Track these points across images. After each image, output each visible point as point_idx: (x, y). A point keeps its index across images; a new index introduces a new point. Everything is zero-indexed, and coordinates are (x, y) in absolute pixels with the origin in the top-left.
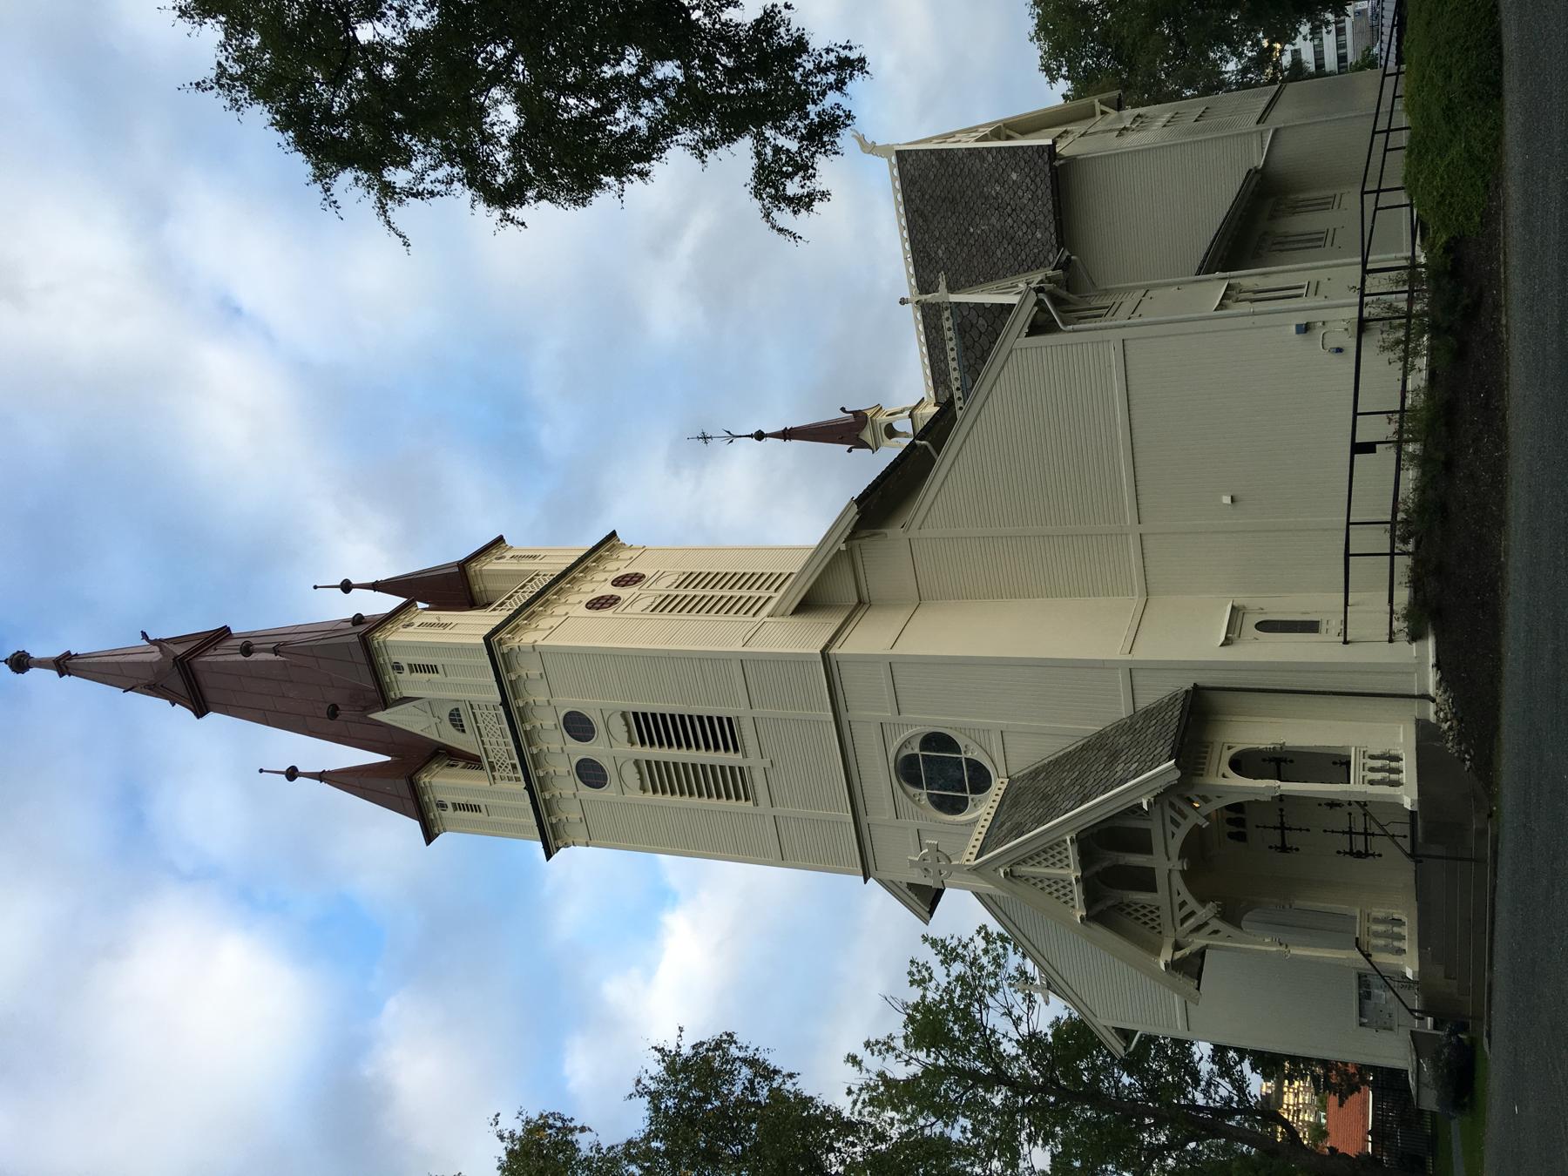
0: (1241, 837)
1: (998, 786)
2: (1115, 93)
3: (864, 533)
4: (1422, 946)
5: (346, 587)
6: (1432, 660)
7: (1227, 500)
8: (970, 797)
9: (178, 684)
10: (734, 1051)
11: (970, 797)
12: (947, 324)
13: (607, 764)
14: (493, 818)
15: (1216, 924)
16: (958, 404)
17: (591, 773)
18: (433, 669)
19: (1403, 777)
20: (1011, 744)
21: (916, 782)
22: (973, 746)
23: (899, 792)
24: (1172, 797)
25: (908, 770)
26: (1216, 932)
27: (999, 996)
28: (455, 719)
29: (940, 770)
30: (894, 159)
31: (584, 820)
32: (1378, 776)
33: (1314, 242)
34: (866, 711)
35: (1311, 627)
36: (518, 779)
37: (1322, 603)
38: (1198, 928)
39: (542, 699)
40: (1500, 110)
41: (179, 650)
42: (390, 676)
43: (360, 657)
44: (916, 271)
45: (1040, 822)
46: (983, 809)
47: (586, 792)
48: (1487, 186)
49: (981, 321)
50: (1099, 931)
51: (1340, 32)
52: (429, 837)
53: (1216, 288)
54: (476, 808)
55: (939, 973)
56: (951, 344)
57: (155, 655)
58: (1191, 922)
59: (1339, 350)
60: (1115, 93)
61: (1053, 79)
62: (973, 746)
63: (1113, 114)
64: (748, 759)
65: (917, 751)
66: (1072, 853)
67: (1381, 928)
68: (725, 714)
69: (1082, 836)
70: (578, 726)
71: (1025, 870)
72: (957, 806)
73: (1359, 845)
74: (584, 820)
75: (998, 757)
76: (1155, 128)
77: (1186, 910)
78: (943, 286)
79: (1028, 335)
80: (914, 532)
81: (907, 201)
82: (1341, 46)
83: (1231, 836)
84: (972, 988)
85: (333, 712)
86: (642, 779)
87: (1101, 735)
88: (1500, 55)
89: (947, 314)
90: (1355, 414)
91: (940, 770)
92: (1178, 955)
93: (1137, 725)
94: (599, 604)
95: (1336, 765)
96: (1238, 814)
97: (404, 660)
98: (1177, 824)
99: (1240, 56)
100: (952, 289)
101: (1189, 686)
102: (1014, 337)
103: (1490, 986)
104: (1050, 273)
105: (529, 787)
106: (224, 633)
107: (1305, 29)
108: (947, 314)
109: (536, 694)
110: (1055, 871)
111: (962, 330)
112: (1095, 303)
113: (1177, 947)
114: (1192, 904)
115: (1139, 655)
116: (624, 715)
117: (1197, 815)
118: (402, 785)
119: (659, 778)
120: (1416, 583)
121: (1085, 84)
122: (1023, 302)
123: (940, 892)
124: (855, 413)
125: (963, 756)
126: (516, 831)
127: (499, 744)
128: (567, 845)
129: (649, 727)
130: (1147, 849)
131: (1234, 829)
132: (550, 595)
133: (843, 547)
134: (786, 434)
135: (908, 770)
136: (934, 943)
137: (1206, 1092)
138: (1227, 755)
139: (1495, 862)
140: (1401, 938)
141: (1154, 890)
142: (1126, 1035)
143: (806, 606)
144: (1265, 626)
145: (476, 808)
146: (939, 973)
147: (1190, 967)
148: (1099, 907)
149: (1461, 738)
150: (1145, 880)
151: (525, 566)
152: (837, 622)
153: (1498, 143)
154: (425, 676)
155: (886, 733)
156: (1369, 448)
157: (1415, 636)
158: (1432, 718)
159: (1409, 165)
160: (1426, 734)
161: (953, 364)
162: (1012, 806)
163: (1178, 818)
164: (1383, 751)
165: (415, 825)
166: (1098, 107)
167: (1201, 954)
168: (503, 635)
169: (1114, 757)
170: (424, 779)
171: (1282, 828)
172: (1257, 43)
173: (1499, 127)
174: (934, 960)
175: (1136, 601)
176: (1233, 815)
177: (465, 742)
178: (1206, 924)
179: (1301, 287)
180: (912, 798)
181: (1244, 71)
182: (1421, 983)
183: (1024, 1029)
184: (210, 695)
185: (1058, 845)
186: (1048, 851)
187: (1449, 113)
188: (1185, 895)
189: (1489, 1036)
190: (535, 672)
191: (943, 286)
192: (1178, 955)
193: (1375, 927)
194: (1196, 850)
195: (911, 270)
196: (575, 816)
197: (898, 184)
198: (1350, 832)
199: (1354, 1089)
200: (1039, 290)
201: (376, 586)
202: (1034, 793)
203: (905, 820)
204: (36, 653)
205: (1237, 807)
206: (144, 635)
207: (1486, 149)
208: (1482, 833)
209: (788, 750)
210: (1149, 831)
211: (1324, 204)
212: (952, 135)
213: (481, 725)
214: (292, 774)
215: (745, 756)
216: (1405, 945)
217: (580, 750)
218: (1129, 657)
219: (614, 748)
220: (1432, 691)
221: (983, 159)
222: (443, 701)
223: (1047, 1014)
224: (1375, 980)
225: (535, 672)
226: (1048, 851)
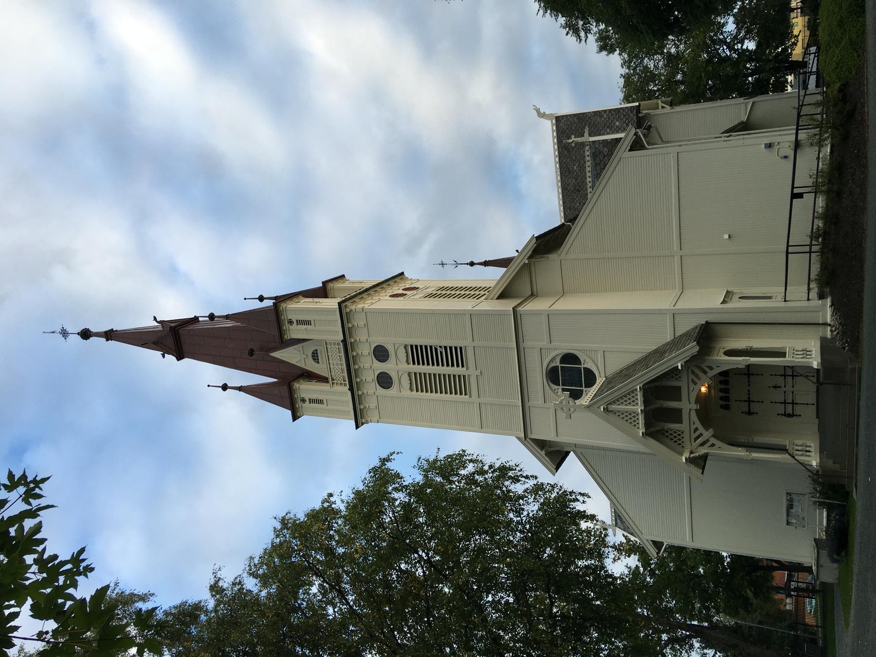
0: (726, 407)
1: (600, 381)
2: (670, 99)
7: (726, 236)
8: (585, 389)
9: (170, 342)
11: (585, 389)
12: (587, 153)
13: (394, 375)
14: (330, 407)
15: (713, 440)
17: (385, 381)
18: (308, 323)
21: (589, 372)
22: (588, 360)
23: (547, 387)
25: (553, 375)
26: (713, 445)
28: (315, 356)
29: (570, 375)
30: (554, 121)
31: (378, 407)
34: (534, 342)
36: (345, 385)
39: (363, 338)
42: (286, 326)
43: (273, 317)
44: (561, 178)
47: (381, 391)
48: (859, 56)
49: (605, 149)
52: (295, 418)
56: (588, 164)
59: (786, 157)
60: (670, 99)
62: (588, 360)
64: (469, 371)
65: (558, 364)
66: (640, 397)
68: (458, 345)
69: (647, 386)
70: (381, 353)
71: (614, 407)
73: (789, 411)
74: (378, 407)
75: (601, 368)
77: (698, 433)
78: (586, 134)
79: (630, 150)
80: (563, 256)
83: (722, 407)
85: (251, 353)
86: (411, 384)
89: (587, 148)
91: (570, 375)
92: (692, 455)
97: (294, 318)
98: (695, 397)
100: (590, 135)
102: (623, 153)
103: (857, 454)
105: (351, 389)
108: (587, 148)
109: (361, 336)
111: (594, 156)
113: (691, 453)
114: (701, 429)
119: (421, 383)
125: (582, 366)
127: (336, 365)
128: (367, 422)
129: (419, 354)
131: (723, 395)
132: (371, 292)
133: (527, 262)
138: (722, 351)
142: (658, 545)
143: (502, 296)
148: (653, 429)
150: (676, 416)
152: (527, 280)
153: (864, 33)
154: (304, 327)
155: (543, 352)
158: (829, 336)
161: (589, 174)
163: (696, 379)
166: (660, 104)
167: (705, 457)
168: (347, 303)
170: (296, 385)
173: (864, 25)
175: (677, 292)
176: (723, 378)
178: (707, 441)
180: (553, 391)
185: (632, 392)
188: (698, 424)
189: (856, 486)
190: (361, 323)
191: (586, 134)
192: (692, 455)
193: (797, 448)
195: (559, 178)
197: (555, 134)
198: (785, 403)
204: (94, 329)
205: (725, 374)
206: (155, 319)
207: (858, 36)
210: (680, 387)
213: (330, 354)
214: (225, 387)
219: (398, 366)
220: (829, 322)
221: (602, 116)
225: (361, 323)
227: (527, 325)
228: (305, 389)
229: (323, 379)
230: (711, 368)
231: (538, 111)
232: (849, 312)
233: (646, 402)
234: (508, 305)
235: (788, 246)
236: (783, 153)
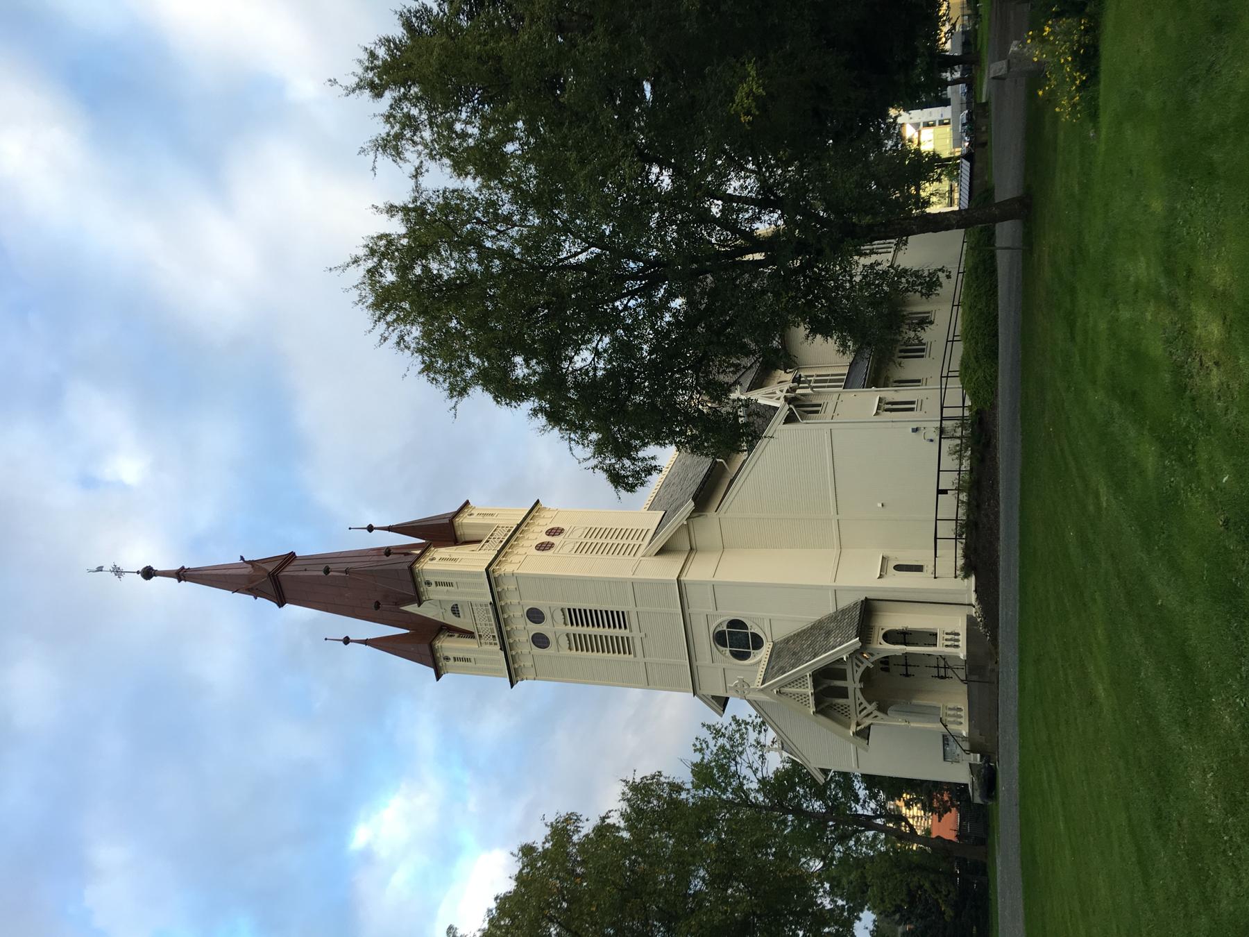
4: (970, 721)
5: (370, 528)
9: (270, 588)
10: (662, 779)
17: (540, 641)
18: (450, 584)
19: (960, 637)
20: (774, 625)
21: (755, 636)
24: (856, 654)
27: (744, 756)
28: (455, 610)
29: (737, 639)
31: (534, 666)
32: (949, 643)
35: (919, 568)
37: (922, 555)
38: (868, 715)
39: (515, 601)
40: (997, 364)
41: (270, 568)
42: (423, 588)
45: (794, 667)
46: (763, 654)
47: (537, 651)
50: (821, 718)
52: (438, 677)
54: (468, 660)
55: (711, 743)
57: (249, 569)
64: (632, 633)
66: (809, 681)
67: (952, 713)
70: (535, 616)
73: (942, 672)
74: (534, 666)
84: (729, 754)
85: (377, 605)
87: (820, 622)
93: (839, 616)
94: (543, 547)
95: (930, 637)
96: (886, 662)
97: (432, 579)
102: (777, 426)
105: (503, 648)
106: (292, 556)
112: (815, 402)
113: (858, 725)
114: (865, 704)
115: (720, 577)
116: (562, 610)
117: (868, 662)
118: (425, 648)
119: (580, 643)
120: (965, 556)
123: (727, 699)
126: (494, 672)
127: (486, 624)
129: (575, 616)
130: (845, 678)
134: (181, 575)
135: (720, 638)
136: (709, 727)
137: (863, 807)
138: (882, 633)
140: (961, 717)
141: (847, 697)
142: (825, 772)
144: (899, 568)
145: (468, 660)
146: (711, 743)
147: (864, 734)
149: (985, 626)
150: (843, 693)
151: (488, 520)
154: (446, 588)
156: (945, 492)
157: (966, 576)
160: (971, 621)
164: (950, 628)
165: (431, 671)
167: (869, 727)
168: (494, 567)
169: (828, 633)
171: (906, 665)
174: (709, 738)
175: (836, 552)
177: (461, 623)
179: (913, 403)
182: (969, 739)
183: (759, 775)
184: (287, 595)
186: (798, 680)
188: (862, 699)
190: (512, 587)
194: (867, 677)
196: (528, 663)
199: (947, 810)
201: (390, 529)
202: (787, 652)
203: (719, 667)
209: (657, 630)
214: (347, 641)
216: (962, 720)
217: (535, 628)
220: (973, 602)
222: (448, 601)
223: (775, 762)
224: (951, 739)
225: (512, 587)
226: (798, 680)
227: (692, 595)
228: (447, 645)
229: (470, 635)
232: (987, 594)
233: (815, 687)
234: (668, 569)
235: (942, 408)
236: (929, 436)
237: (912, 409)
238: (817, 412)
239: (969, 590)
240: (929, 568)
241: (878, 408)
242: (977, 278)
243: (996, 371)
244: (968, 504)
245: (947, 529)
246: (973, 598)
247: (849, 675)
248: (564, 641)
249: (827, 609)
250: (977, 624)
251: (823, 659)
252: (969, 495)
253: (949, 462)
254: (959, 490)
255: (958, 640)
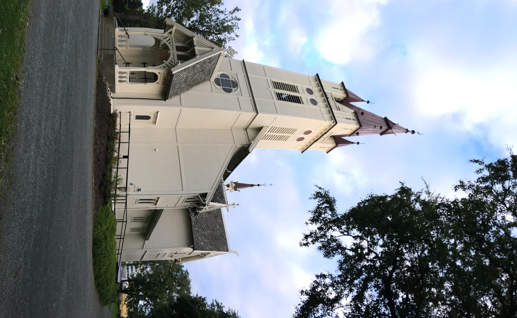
3: (246, 146)
4: (114, 38)
6: (112, 106)
7: (157, 150)
15: (161, 39)
16: (222, 179)
17: (310, 91)
18: (347, 118)
20: (208, 89)
25: (235, 85)
29: (227, 84)
31: (310, 82)
33: (136, 220)
34: (246, 99)
35: (138, 117)
37: (137, 125)
40: (93, 236)
41: (390, 131)
42: (355, 118)
46: (216, 74)
47: (311, 88)
51: (128, 275)
53: (159, 206)
58: (168, 39)
59: (131, 184)
61: (314, 220)
63: (177, 259)
66: (197, 52)
68: (280, 101)
70: (314, 102)
72: (222, 75)
74: (310, 82)
76: (166, 254)
77: (169, 42)
79: (207, 193)
80: (234, 145)
81: (226, 240)
82: (128, 272)
88: (93, 251)
90: (127, 168)
91: (227, 84)
92: (171, 30)
97: (352, 121)
99: (147, 271)
101: (167, 100)
104: (200, 211)
107: (135, 276)
110: (201, 48)
112: (188, 203)
114: (167, 43)
119: (293, 88)
121: (179, 268)
122: (208, 203)
124: (236, 190)
129: (297, 100)
130: (178, 55)
134: (252, 185)
135: (235, 85)
138: (158, 81)
139: (98, 48)
143: (259, 129)
144: (148, 118)
149: (105, 85)
150: (178, 49)
156: (125, 157)
159: (116, 227)
160: (113, 90)
162: (211, 70)
164: (123, 87)
168: (333, 124)
172: (143, 274)
175: (178, 127)
179: (140, 203)
181: (146, 268)
186: (203, 53)
187: (106, 238)
188: (169, 45)
196: (312, 83)
200: (204, 205)
208: (101, 56)
211: (133, 230)
212: (215, 255)
215: (274, 91)
218: (182, 108)
219: (305, 96)
220: (112, 99)
221: (209, 248)
227: (250, 106)
230: (164, 67)
231: (237, 254)
233: (194, 50)
236: (132, 186)
237: (140, 200)
238: (188, 199)
239: (114, 105)
240: (133, 117)
241: (157, 201)
242: (107, 281)
243: (94, 231)
244: (113, 150)
245: (124, 137)
246: (112, 101)
247: (176, 57)
248: (300, 89)
249: (184, 95)
250: (110, 87)
251: (190, 64)
252: (113, 155)
253: (122, 173)
254: (118, 158)
255: (120, 77)
